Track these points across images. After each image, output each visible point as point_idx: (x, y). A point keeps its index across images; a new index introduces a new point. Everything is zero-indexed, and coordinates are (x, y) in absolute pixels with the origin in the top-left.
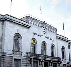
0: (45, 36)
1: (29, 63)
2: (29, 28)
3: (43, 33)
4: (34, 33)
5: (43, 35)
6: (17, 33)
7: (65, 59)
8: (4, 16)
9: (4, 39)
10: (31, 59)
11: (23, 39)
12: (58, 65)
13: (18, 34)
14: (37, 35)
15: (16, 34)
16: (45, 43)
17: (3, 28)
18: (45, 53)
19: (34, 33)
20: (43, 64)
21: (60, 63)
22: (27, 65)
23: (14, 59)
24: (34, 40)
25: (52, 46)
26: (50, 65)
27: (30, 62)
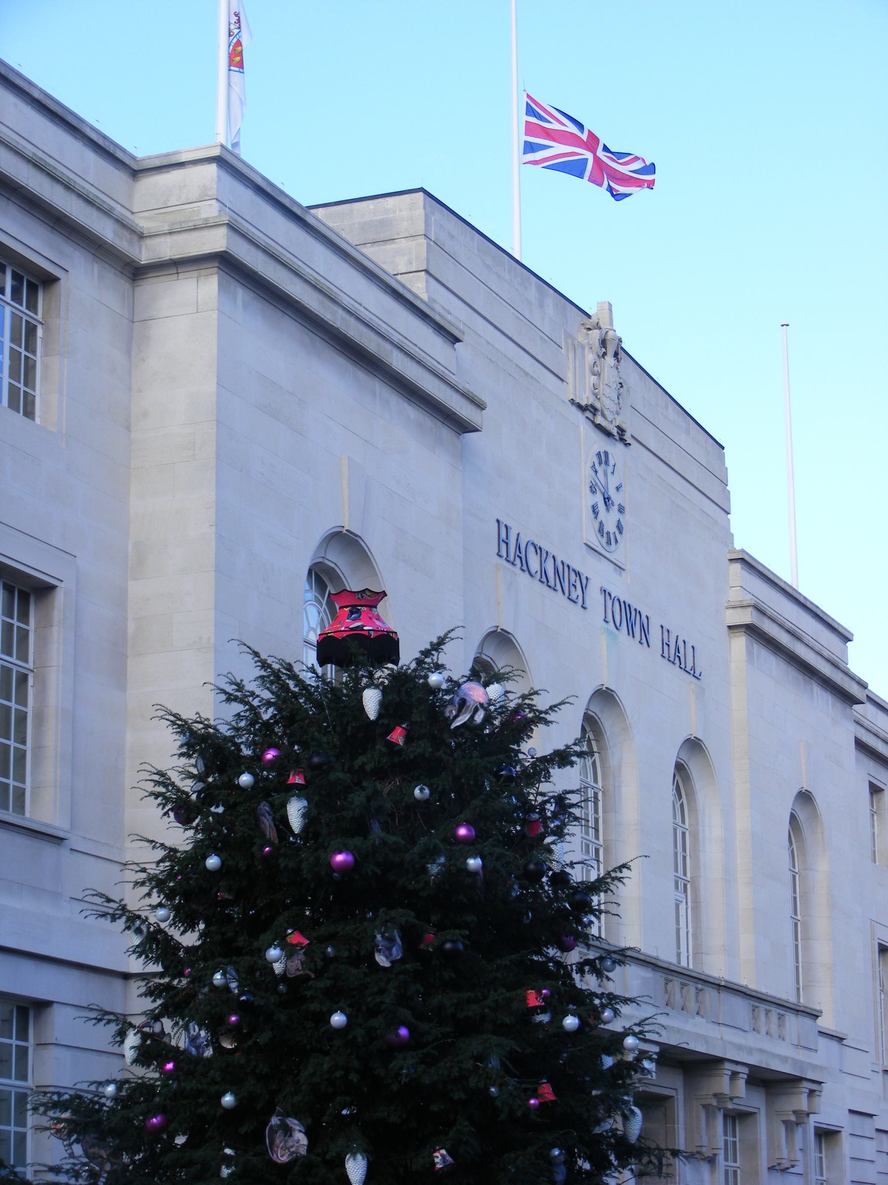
14: (534, 563)
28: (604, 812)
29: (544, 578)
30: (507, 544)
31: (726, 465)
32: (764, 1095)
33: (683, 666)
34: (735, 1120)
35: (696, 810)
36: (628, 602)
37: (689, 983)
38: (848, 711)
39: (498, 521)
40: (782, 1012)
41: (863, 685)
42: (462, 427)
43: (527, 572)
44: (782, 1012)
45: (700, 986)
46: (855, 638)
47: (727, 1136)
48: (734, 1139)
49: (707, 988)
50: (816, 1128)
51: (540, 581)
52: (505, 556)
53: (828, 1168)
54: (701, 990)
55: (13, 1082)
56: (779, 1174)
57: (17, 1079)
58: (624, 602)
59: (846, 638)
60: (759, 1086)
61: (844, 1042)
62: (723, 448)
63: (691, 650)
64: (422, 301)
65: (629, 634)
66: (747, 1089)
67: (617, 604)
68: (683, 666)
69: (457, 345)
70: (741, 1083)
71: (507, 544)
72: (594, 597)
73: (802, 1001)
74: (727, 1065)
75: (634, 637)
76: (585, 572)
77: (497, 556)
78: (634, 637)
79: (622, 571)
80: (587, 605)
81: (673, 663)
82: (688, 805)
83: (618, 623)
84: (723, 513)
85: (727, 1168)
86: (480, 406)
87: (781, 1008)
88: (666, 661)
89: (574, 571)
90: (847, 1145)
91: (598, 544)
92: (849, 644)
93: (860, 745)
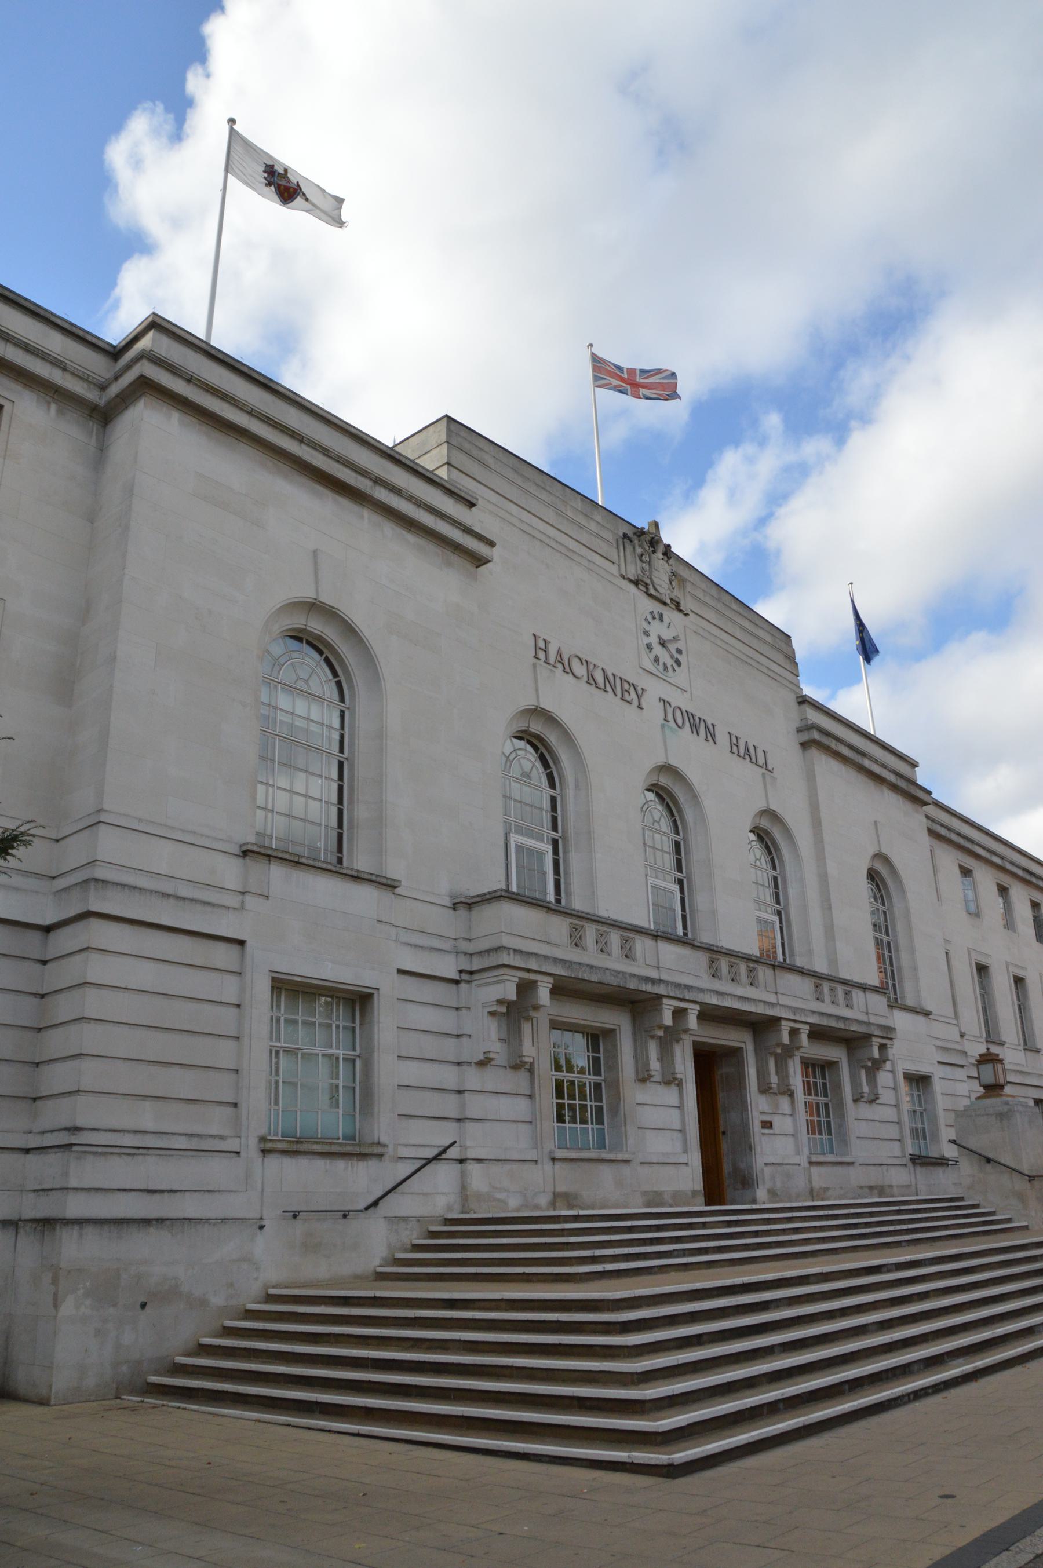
0: (678, 700)
1: (498, 1049)
2: (480, 561)
3: (650, 666)
4: (541, 648)
5: (654, 689)
6: (314, 607)
7: (910, 1002)
8: (115, 353)
9: (113, 659)
10: (526, 988)
11: (708, 803)
12: (762, 1074)
13: (316, 626)
14: (580, 670)
15: (299, 621)
16: (552, 738)
17: (91, 517)
18: (267, 791)
19: (541, 648)
20: (685, 1066)
21: (883, 1060)
22: (473, 1079)
23: (262, 988)
24: (317, 644)
25: (1009, 924)
26: (643, 1078)
27: (512, 1036)
28: (685, 854)
29: (591, 680)
30: (737, 746)
31: (794, 647)
32: (846, 1050)
33: (754, 760)
34: (281, 992)
35: (783, 861)
36: (691, 710)
37: (718, 957)
38: (920, 809)
39: (729, 733)
40: (849, 989)
41: (929, 793)
42: (480, 561)
43: (571, 675)
44: (849, 989)
45: (752, 965)
46: (920, 765)
47: (816, 1078)
48: (354, 1025)
49: (741, 962)
50: (904, 1073)
51: (587, 682)
52: (736, 753)
53: (925, 1101)
54: (754, 968)
55: (813, 1097)
56: (867, 1105)
57: (567, 1072)
58: (686, 711)
59: (914, 765)
60: (841, 1043)
61: (397, 891)
62: (790, 637)
63: (763, 753)
64: (445, 480)
65: (693, 732)
66: (809, 1041)
67: (678, 714)
68: (754, 760)
69: (473, 509)
70: (804, 1038)
71: (737, 746)
72: (650, 700)
73: (788, 961)
74: (874, 1039)
75: (698, 735)
76: (640, 685)
77: (563, 673)
78: (698, 735)
79: (685, 693)
80: (644, 705)
81: (605, 691)
82: (778, 858)
83: (680, 722)
84: (795, 677)
85: (272, 1048)
86: (491, 544)
87: (605, 926)
88: (735, 756)
89: (626, 681)
90: (938, 1086)
91: (655, 670)
92: (916, 769)
93: (931, 832)
